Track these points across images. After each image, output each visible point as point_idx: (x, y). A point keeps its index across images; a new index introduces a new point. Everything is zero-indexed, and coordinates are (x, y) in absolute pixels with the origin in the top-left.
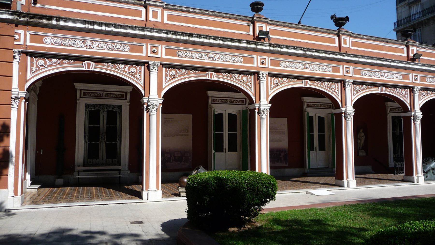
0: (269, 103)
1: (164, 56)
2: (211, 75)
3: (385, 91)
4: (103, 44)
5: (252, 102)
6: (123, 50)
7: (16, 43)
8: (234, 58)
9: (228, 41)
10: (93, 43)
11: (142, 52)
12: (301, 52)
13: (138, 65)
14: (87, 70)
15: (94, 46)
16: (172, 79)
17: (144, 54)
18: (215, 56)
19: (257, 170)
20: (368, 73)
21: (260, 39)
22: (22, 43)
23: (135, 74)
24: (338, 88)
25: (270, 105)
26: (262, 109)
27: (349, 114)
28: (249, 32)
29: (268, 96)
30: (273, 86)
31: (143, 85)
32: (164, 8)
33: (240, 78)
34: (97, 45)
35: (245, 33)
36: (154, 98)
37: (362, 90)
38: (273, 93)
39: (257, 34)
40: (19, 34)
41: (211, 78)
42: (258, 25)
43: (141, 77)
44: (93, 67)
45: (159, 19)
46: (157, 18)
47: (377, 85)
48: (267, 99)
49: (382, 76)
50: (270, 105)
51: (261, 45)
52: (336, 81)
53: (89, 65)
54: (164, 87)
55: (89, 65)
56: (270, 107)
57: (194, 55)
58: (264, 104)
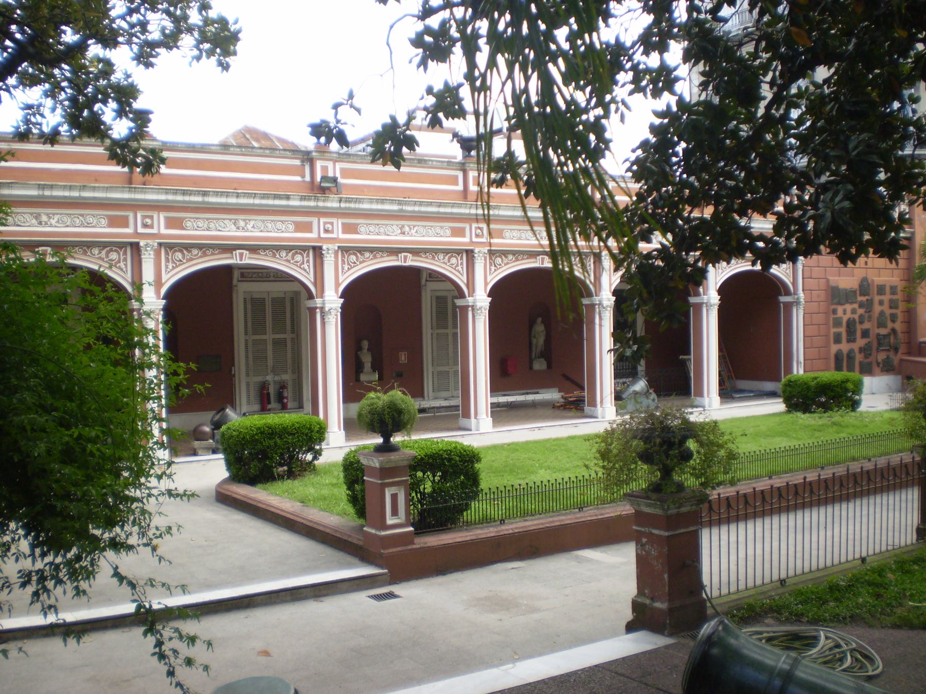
0: (341, 297)
2: (241, 255)
3: (411, 261)
4: (65, 219)
5: (462, 295)
8: (279, 225)
9: (268, 198)
10: (50, 218)
11: (464, 236)
12: (395, 207)
13: (121, 248)
14: (239, 262)
15: (249, 227)
16: (177, 266)
18: (246, 224)
19: (795, 372)
20: (515, 234)
21: (323, 190)
23: (117, 263)
24: (462, 264)
25: (490, 299)
26: (327, 309)
27: (480, 308)
28: (303, 176)
29: (337, 284)
30: (346, 267)
31: (465, 281)
32: (335, 161)
34: (56, 219)
35: (298, 178)
37: (506, 265)
38: (346, 279)
39: (319, 179)
41: (241, 260)
42: (319, 164)
43: (126, 267)
47: (395, 252)
48: (337, 291)
49: (40, 223)
50: (490, 299)
51: (324, 201)
54: (163, 281)
56: (342, 305)
57: (212, 225)
58: (481, 299)
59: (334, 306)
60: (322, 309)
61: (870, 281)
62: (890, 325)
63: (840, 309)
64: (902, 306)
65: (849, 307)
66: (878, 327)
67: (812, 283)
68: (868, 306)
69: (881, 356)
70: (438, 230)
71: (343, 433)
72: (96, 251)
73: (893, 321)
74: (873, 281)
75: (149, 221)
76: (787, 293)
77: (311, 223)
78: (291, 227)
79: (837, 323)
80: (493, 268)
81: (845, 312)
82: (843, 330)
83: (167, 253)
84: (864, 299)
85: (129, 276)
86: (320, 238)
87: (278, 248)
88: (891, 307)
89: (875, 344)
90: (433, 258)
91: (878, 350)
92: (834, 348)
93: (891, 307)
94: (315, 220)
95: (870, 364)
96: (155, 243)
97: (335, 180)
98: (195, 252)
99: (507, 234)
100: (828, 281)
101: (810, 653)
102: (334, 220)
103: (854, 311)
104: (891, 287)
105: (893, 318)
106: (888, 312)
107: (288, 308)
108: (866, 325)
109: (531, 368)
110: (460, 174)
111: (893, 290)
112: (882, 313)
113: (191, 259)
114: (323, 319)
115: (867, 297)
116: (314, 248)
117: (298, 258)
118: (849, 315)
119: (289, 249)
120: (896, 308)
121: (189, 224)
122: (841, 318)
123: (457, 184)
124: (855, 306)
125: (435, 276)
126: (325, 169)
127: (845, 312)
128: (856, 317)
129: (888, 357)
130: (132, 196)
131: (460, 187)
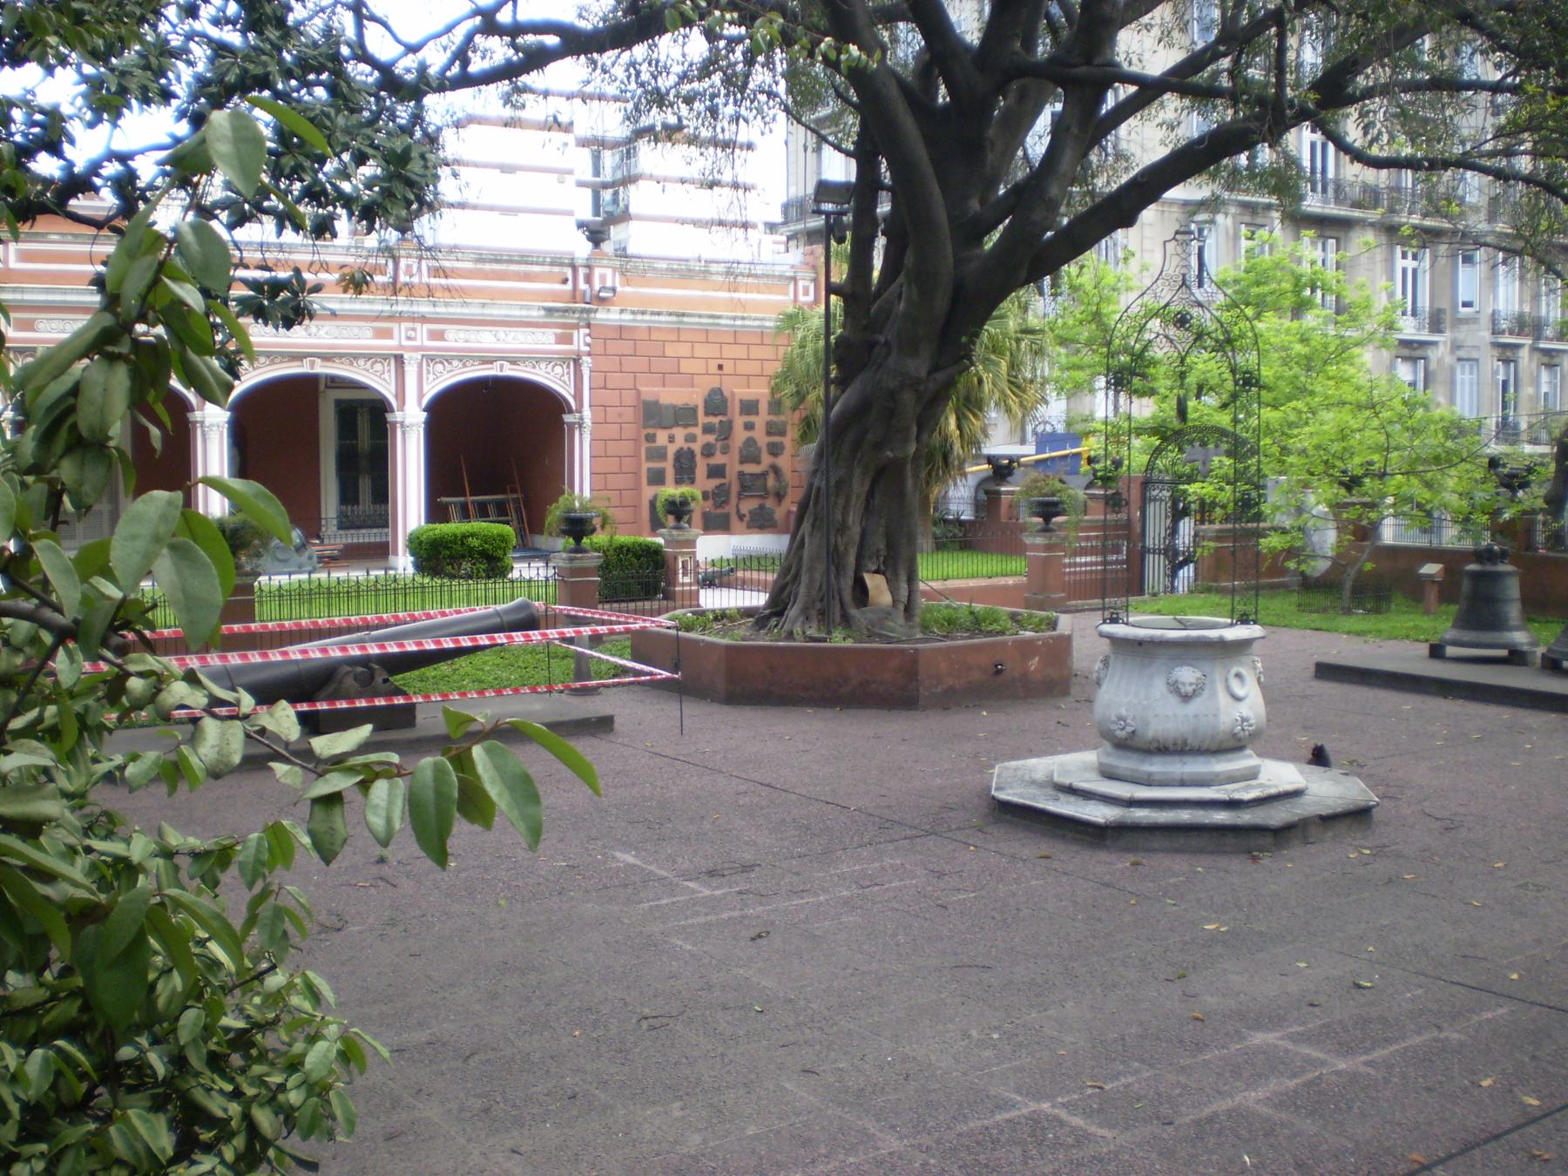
15: (322, 333)
21: (602, 301)
29: (421, 395)
48: (419, 403)
52: (385, 357)
55: (312, 365)
59: (414, 421)
60: (402, 423)
61: (726, 394)
62: (767, 459)
63: (662, 437)
65: (680, 433)
66: (741, 463)
67: (610, 397)
68: (726, 431)
69: (748, 506)
70: (356, 331)
72: (362, 362)
74: (733, 394)
75: (412, 334)
76: (570, 411)
78: (369, 333)
79: (660, 454)
80: (431, 377)
81: (672, 440)
82: (669, 466)
84: (715, 420)
85: (393, 388)
86: (401, 347)
87: (356, 357)
88: (769, 434)
89: (735, 488)
91: (740, 497)
92: (648, 492)
93: (769, 434)
94: (395, 326)
95: (727, 517)
96: (418, 355)
97: (614, 290)
100: (639, 393)
102: (418, 326)
103: (691, 438)
105: (775, 450)
106: (762, 439)
107: (367, 419)
108: (718, 459)
112: (750, 442)
114: (404, 433)
115: (720, 418)
118: (680, 442)
119: (368, 357)
121: (41, 326)
122: (665, 448)
124: (698, 431)
125: (335, 382)
126: (603, 278)
127: (672, 439)
128: (696, 448)
129: (762, 507)
130: (466, 310)
131: (569, 286)
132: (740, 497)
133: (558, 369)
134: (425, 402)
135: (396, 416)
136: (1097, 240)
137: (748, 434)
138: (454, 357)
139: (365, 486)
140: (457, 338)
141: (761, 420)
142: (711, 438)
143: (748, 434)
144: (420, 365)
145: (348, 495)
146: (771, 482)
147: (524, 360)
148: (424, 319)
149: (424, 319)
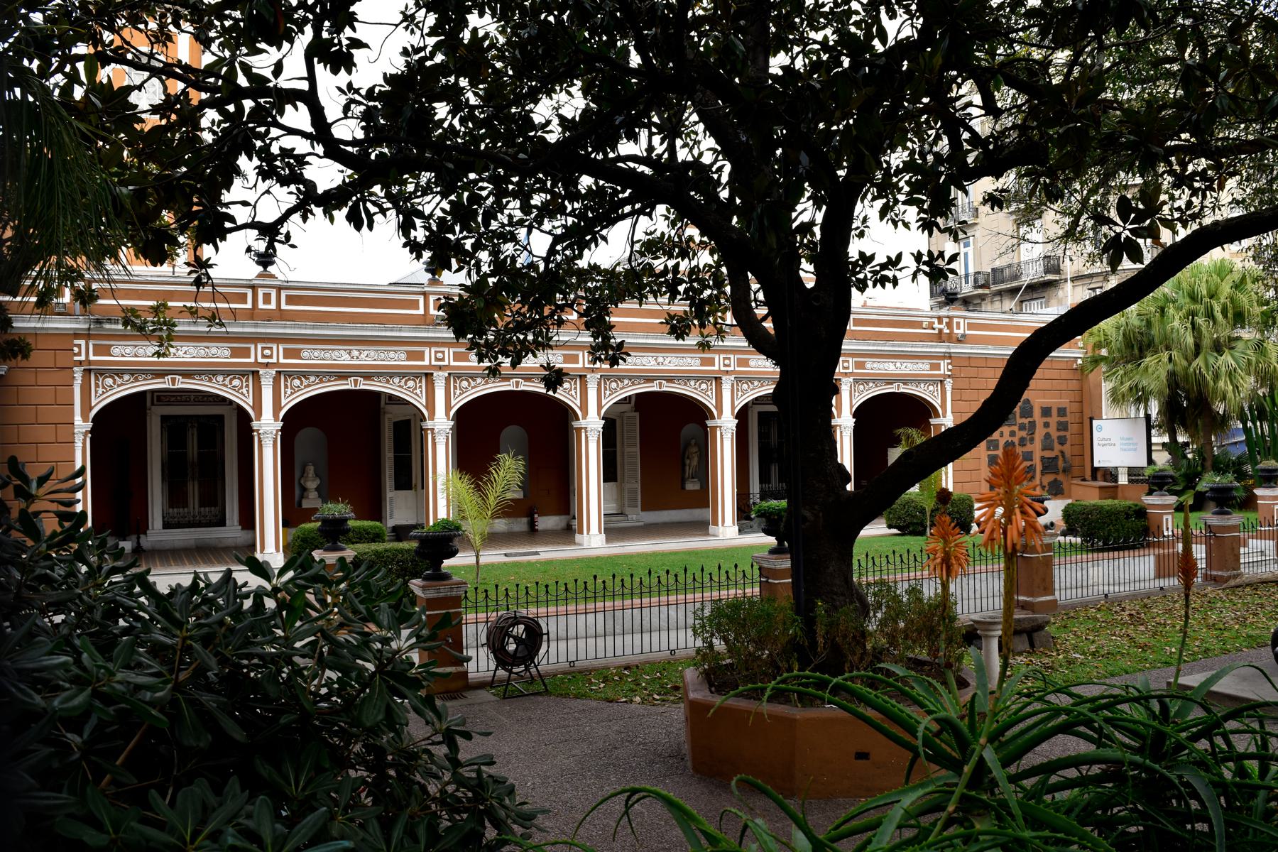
1: (282, 360)
2: (356, 381)
3: (364, 385)
6: (396, 358)
7: (76, 358)
8: (392, 355)
11: (249, 357)
15: (363, 356)
17: (252, 360)
22: (83, 358)
29: (733, 408)
30: (458, 392)
33: (227, 382)
36: (268, 425)
40: (79, 346)
44: (182, 383)
45: (273, 306)
46: (269, 303)
48: (599, 414)
52: (709, 379)
53: (173, 380)
55: (173, 380)
64: (1073, 428)
71: (603, 536)
72: (396, 380)
73: (1062, 444)
76: (937, 415)
77: (249, 349)
78: (403, 356)
83: (286, 380)
84: (1026, 421)
88: (1058, 430)
89: (1039, 468)
90: (388, 382)
93: (1058, 430)
98: (312, 378)
99: (868, 366)
101: (921, 792)
103: (1013, 434)
104: (1059, 410)
105: (1062, 441)
109: (683, 488)
110: (249, 293)
111: (1062, 412)
113: (309, 386)
116: (426, 375)
117: (236, 382)
118: (1007, 438)
120: (1066, 429)
123: (418, 308)
124: (1015, 428)
127: (1002, 435)
128: (1016, 440)
132: (1042, 474)
133: (931, 388)
134: (282, 414)
135: (428, 424)
136: (1184, 266)
137: (1046, 430)
138: (311, 374)
139: (193, 490)
140: (313, 357)
141: (1054, 419)
142: (1024, 434)
143: (1046, 430)
144: (599, 384)
145: (175, 497)
146: (1061, 464)
147: (379, 375)
148: (278, 339)
149: (278, 339)
